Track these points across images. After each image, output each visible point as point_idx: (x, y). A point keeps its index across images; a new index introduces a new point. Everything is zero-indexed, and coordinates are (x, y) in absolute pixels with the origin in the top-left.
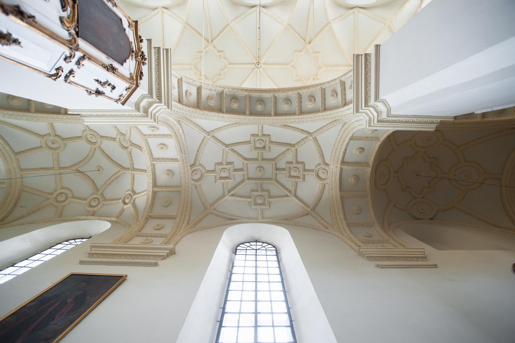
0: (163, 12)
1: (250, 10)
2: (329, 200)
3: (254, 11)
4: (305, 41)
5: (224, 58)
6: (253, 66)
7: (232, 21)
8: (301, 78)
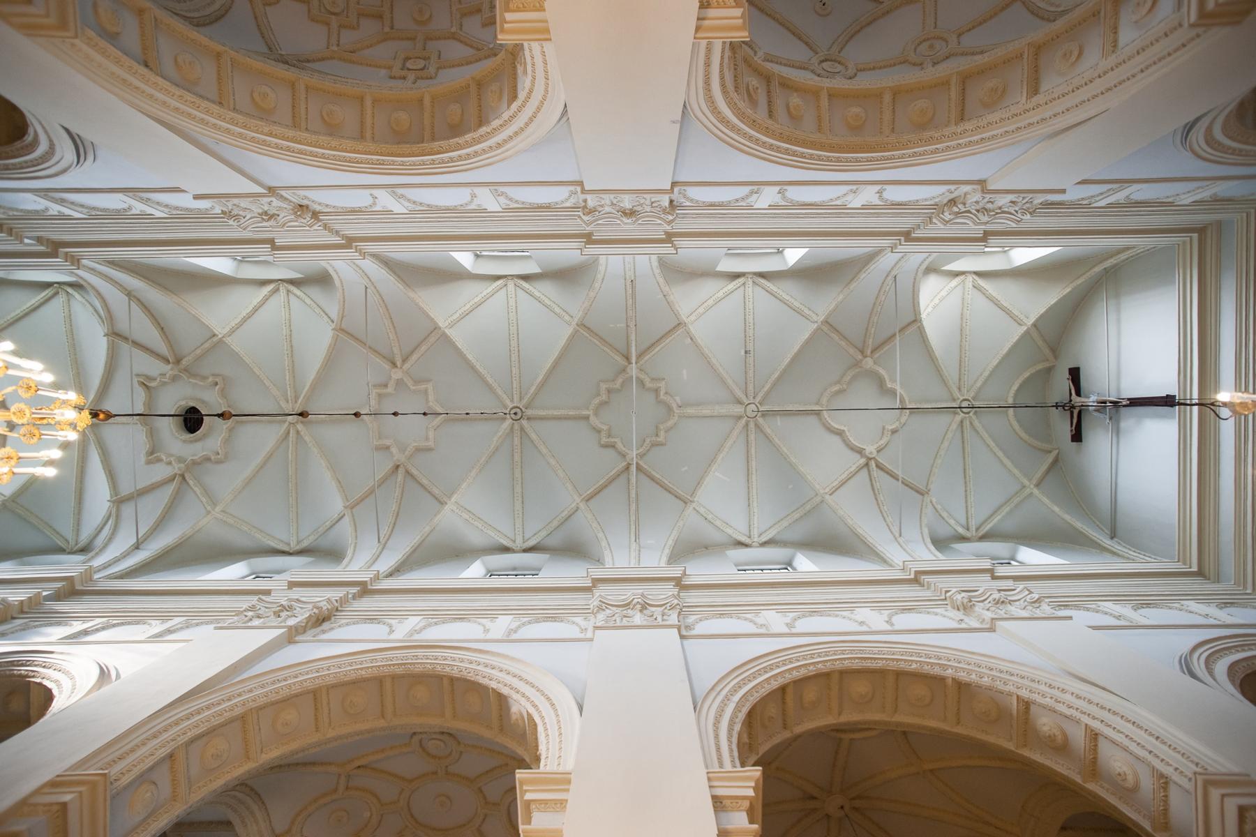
0: (750, 537)
1: (538, 540)
2: (637, 519)
3: (528, 539)
4: (407, 472)
5: (599, 431)
6: (529, 412)
7: (577, 509)
8: (414, 388)
